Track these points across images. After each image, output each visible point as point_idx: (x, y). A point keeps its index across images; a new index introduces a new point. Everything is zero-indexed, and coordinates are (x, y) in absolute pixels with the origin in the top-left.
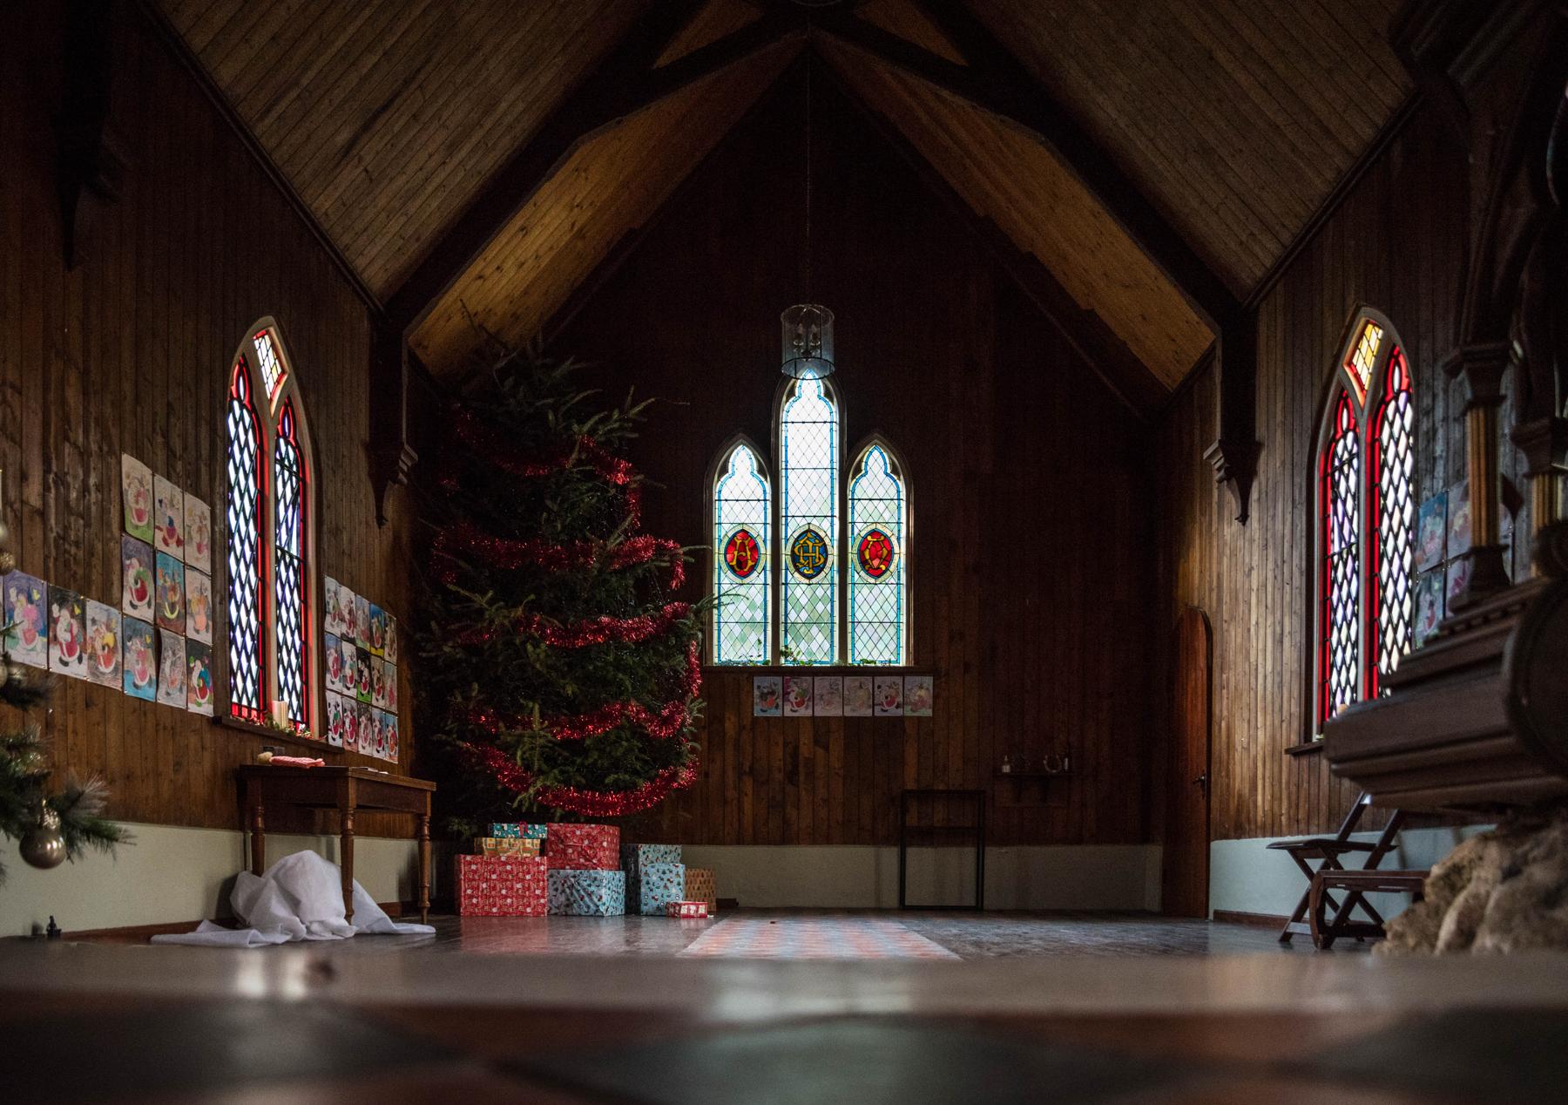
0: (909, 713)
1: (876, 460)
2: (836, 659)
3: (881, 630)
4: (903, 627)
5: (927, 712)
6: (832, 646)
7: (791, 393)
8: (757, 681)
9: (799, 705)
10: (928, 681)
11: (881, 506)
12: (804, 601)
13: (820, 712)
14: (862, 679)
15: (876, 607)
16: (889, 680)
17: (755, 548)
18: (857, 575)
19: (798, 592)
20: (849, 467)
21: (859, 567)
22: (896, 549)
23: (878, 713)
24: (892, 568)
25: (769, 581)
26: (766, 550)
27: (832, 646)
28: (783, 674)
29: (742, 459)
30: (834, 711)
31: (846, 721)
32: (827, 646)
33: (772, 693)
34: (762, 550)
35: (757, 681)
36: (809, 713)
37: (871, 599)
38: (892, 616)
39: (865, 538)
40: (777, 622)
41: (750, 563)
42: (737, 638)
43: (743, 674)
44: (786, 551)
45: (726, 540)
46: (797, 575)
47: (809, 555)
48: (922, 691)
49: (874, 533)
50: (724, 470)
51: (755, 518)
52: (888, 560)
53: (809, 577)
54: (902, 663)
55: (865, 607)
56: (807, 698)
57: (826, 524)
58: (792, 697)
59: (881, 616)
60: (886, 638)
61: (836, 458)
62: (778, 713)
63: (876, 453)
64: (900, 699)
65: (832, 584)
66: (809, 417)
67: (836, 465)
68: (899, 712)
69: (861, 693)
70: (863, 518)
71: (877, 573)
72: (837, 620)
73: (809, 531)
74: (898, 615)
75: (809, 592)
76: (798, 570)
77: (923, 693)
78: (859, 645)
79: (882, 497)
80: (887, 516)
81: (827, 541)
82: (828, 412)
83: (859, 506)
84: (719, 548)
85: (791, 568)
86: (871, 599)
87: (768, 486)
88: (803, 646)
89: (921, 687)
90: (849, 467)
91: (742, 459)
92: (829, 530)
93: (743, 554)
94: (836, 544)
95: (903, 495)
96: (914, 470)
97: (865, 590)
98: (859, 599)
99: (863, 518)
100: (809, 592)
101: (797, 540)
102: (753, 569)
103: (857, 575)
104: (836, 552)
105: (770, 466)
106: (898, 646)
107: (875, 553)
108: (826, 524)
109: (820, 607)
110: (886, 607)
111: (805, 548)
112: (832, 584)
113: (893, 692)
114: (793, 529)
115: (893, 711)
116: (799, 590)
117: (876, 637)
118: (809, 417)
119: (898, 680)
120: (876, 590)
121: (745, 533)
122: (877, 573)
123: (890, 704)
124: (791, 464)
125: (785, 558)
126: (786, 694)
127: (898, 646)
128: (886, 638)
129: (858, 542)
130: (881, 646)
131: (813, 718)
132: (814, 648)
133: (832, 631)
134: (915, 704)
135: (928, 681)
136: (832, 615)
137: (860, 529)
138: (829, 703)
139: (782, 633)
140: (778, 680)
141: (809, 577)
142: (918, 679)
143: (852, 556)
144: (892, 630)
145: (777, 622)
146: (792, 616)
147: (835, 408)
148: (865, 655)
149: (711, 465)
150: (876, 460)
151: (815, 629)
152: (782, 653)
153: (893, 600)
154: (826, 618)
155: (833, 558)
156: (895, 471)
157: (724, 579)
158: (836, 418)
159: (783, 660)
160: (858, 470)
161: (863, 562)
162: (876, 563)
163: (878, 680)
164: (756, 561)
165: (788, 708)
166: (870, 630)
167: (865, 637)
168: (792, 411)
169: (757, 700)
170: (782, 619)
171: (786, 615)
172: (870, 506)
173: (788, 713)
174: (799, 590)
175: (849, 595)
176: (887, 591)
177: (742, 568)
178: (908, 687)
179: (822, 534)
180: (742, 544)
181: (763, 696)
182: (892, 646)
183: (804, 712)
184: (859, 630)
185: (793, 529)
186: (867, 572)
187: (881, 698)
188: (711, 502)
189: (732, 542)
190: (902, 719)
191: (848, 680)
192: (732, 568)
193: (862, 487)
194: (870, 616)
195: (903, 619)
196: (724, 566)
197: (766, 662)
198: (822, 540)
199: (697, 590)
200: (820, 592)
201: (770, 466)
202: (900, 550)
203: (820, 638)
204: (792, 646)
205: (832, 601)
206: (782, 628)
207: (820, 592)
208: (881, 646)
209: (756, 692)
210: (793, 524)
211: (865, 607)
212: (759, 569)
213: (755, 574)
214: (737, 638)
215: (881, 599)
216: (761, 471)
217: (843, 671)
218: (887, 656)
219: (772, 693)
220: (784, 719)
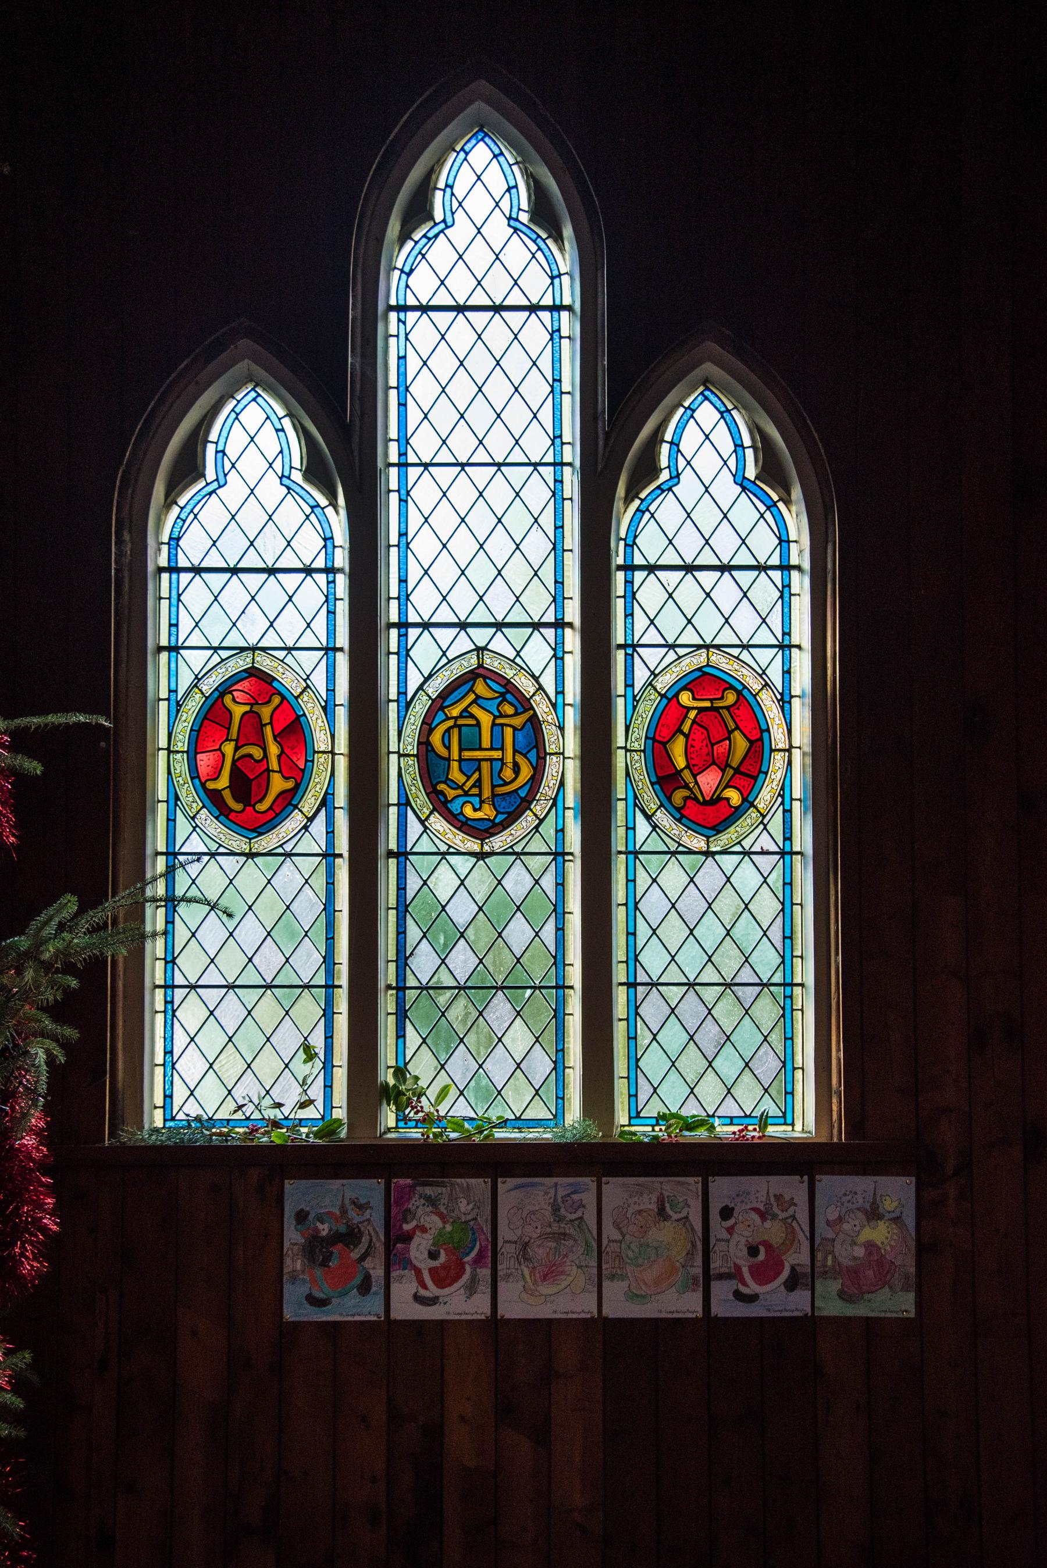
0: (832, 1307)
1: (707, 439)
2: (574, 1113)
3: (727, 1011)
4: (806, 1001)
5: (898, 1303)
6: (559, 1066)
7: (419, 211)
8: (297, 1193)
9: (444, 1277)
10: (897, 1192)
11: (726, 590)
12: (462, 911)
13: (518, 1303)
14: (668, 1185)
15: (710, 932)
16: (760, 1188)
17: (293, 731)
18: (642, 825)
19: (444, 882)
20: (615, 460)
21: (650, 798)
22: (778, 736)
23: (724, 1306)
24: (765, 796)
25: (343, 845)
26: (330, 736)
27: (559, 1066)
28: (384, 1164)
29: (254, 436)
30: (568, 1299)
31: (610, 1336)
32: (541, 1065)
33: (350, 1237)
34: (321, 741)
35: (297, 1193)
36: (478, 1307)
37: (692, 904)
38: (766, 960)
39: (670, 699)
40: (536, 815)
41: (278, 784)
42: (228, 1042)
43: (240, 1174)
44: (400, 738)
45: (193, 706)
46: (438, 823)
47: (476, 756)
48: (875, 1220)
49: (703, 681)
50: (189, 468)
51: (296, 626)
52: (749, 773)
53: (482, 831)
54: (804, 1123)
55: (674, 932)
56: (478, 1252)
57: (537, 652)
58: (418, 1250)
59: (729, 962)
60: (747, 1037)
61: (571, 430)
62: (366, 1309)
63: (707, 413)
64: (799, 1257)
65: (559, 855)
66: (480, 283)
67: (571, 454)
68: (798, 1303)
69: (664, 1234)
70: (668, 623)
71: (711, 817)
72: (575, 975)
73: (479, 673)
74: (785, 960)
75: (481, 881)
76: (441, 805)
77: (880, 1233)
78: (653, 1063)
79: (729, 563)
80: (745, 623)
81: (542, 708)
82: (543, 272)
83: (650, 592)
84: (169, 731)
85: (420, 799)
86: (692, 904)
87: (339, 523)
88: (460, 1065)
89: (873, 1214)
90: (615, 460)
91: (254, 436)
92: (547, 667)
93: (254, 750)
94: (572, 718)
95: (800, 554)
96: (835, 461)
97: (673, 877)
98: (653, 905)
99: (668, 623)
100: (481, 881)
101: (440, 703)
102: (288, 801)
103: (642, 825)
104: (572, 744)
105: (348, 457)
106: (787, 1064)
107: (706, 743)
108: (537, 652)
109: (518, 933)
110: (746, 931)
111: (466, 730)
112: (559, 855)
113: (773, 1232)
114: (423, 663)
115: (777, 1301)
116: (445, 874)
117: (709, 1035)
118: (480, 283)
119: (793, 1187)
120: (709, 876)
121: (260, 681)
122: (711, 817)
123: (764, 1273)
124: (423, 445)
125: (398, 771)
126: (396, 1239)
127: (787, 1064)
128: (747, 1037)
129: (648, 709)
130: (728, 1065)
131: (494, 1325)
132: (496, 1077)
133: (559, 1015)
134: (853, 1273)
135: (897, 1192)
136: (559, 960)
137: (649, 670)
138: (550, 1273)
139: (387, 1025)
140: (371, 1190)
141: (482, 831)
142: (862, 1185)
143: (629, 763)
144: (766, 1011)
145: (367, 986)
146: (424, 964)
147: (566, 261)
148: (672, 1096)
149: (122, 458)
150: (707, 439)
151: (500, 1009)
152: (388, 1094)
153: (767, 906)
154: (539, 969)
155: (565, 768)
156: (772, 472)
157: (181, 827)
158: (570, 293)
159: (389, 1117)
160: (647, 469)
161: (667, 780)
162: (709, 781)
163: (722, 1188)
164: (299, 777)
165: (404, 1290)
166: (691, 1009)
167: (673, 1036)
168: (425, 270)
169: (294, 1263)
170: (388, 974)
171: (403, 960)
172: (689, 592)
173: (405, 1307)
174: (445, 874)
175: (619, 893)
176: (747, 877)
177: (248, 802)
178: (827, 1212)
179: (526, 686)
180: (252, 719)
181: (317, 1250)
182: (768, 1065)
183: (463, 1304)
184: (652, 1009)
185: (423, 663)
186: (681, 815)
187: (731, 1251)
188: (135, 581)
189: (214, 714)
190: (809, 1325)
191: (615, 1188)
192: (215, 799)
193: (658, 528)
194: (691, 960)
195: (806, 972)
196: (188, 794)
197: (329, 1128)
198: (524, 704)
199: (79, 837)
200: (518, 882)
201: (348, 457)
202: (792, 732)
203: (519, 1038)
204: (422, 1067)
205: (559, 911)
206: (387, 1003)
207: (518, 882)
208: (728, 1065)
209: (293, 1236)
210: (425, 652)
211: (674, 932)
212: (309, 802)
213: (294, 822)
214: (228, 1042)
215: (728, 904)
216: (316, 472)
217: (602, 1157)
218: (749, 1098)
219: (350, 1237)
220: (389, 1329)
